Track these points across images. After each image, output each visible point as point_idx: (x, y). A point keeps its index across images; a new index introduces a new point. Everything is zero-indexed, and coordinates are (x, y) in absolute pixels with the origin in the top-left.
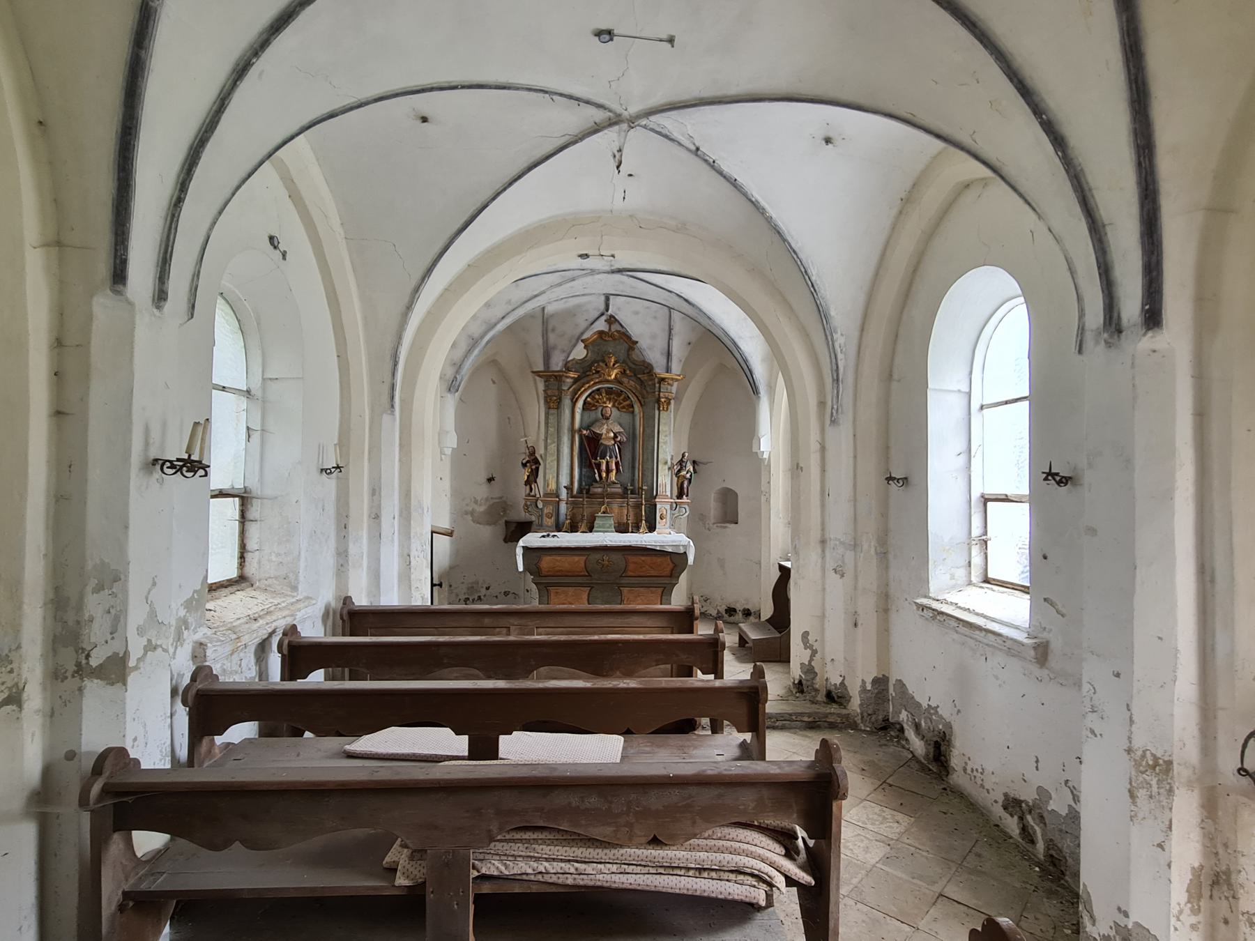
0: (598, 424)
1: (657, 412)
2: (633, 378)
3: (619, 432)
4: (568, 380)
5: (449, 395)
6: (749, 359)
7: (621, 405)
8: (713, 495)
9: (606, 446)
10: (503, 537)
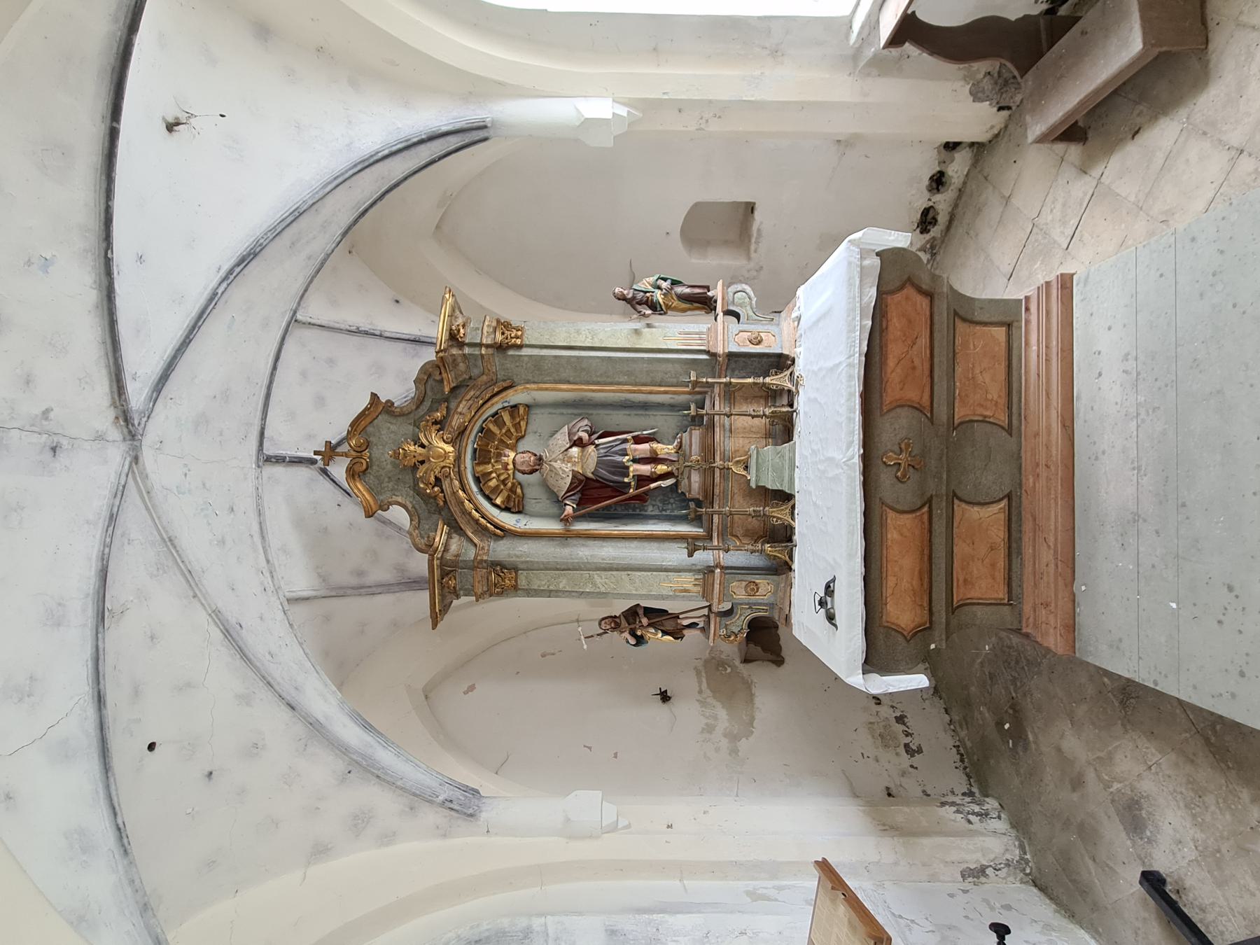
0: (551, 482)
1: (525, 352)
2: (453, 405)
3: (569, 434)
4: (454, 547)
5: (484, 815)
6: (402, 135)
7: (513, 430)
8: (694, 261)
9: (600, 463)
10: (774, 667)
